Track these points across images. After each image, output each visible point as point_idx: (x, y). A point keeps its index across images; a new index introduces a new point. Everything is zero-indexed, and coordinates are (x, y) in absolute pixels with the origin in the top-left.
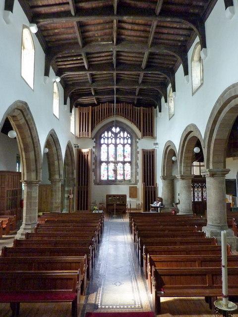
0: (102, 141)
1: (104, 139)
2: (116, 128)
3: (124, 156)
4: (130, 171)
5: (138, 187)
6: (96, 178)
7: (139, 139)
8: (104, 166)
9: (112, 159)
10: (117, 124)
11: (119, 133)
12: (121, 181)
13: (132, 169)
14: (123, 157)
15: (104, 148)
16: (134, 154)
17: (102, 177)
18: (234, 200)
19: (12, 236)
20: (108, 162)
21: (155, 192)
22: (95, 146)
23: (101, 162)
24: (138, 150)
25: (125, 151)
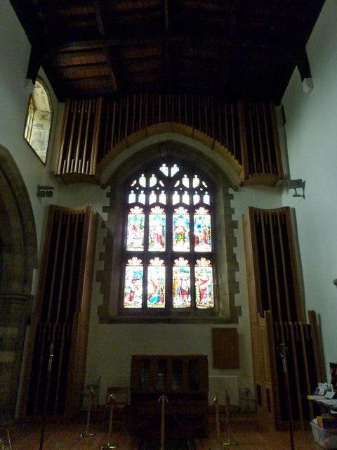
0: (132, 198)
1: (137, 193)
2: (170, 166)
3: (193, 240)
4: (210, 282)
5: (239, 331)
6: (106, 299)
7: (236, 189)
8: (133, 268)
9: (156, 247)
10: (172, 153)
11: (179, 176)
12: (183, 312)
13: (216, 275)
14: (188, 244)
15: (135, 216)
16: (223, 227)
17: (126, 300)
18: (241, 418)
19: (272, 409)
20: (146, 257)
21: (310, 345)
22: (108, 205)
23: (126, 256)
24: (234, 218)
25: (196, 226)
